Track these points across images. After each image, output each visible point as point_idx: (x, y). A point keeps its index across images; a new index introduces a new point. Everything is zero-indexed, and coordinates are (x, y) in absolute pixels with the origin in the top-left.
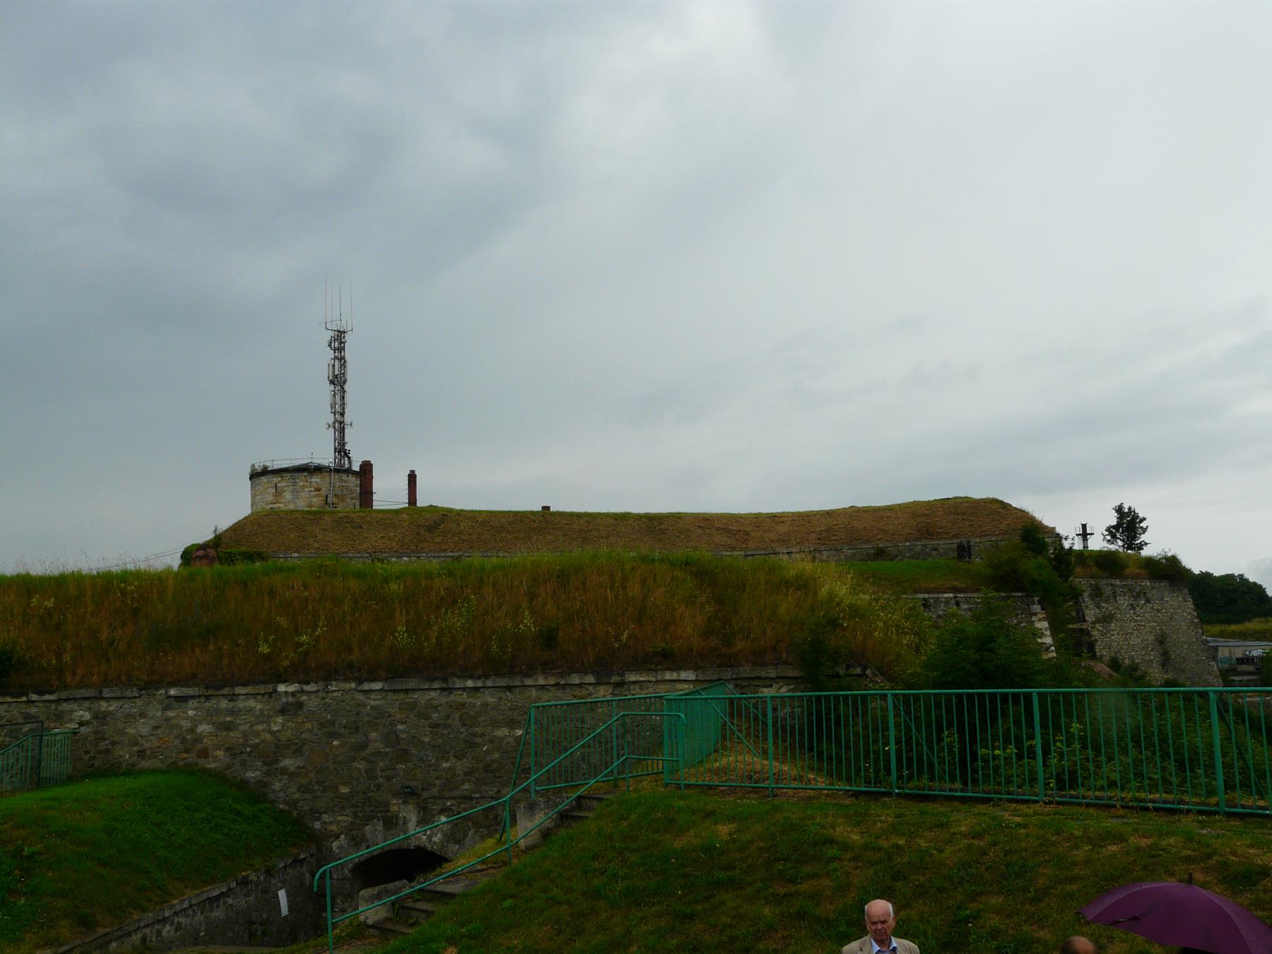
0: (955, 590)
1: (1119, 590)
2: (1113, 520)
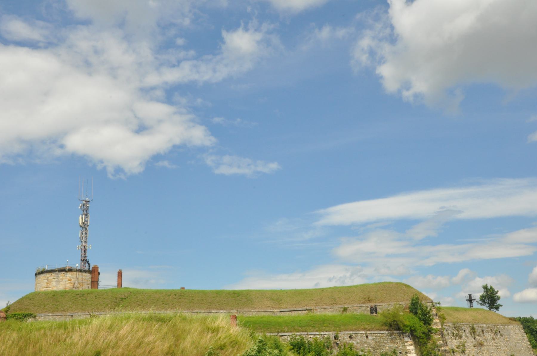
0: (365, 329)
1: (485, 330)
2: (482, 293)
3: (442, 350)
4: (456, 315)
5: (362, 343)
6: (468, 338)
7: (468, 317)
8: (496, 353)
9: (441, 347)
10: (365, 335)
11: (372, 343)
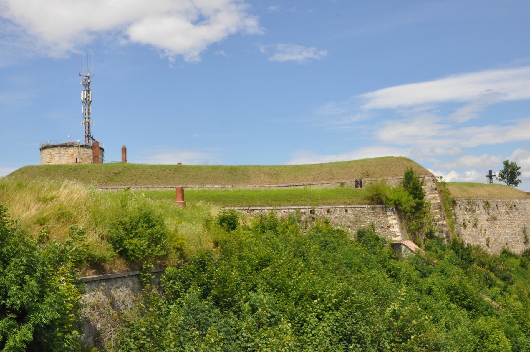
0: (345, 203)
2: (502, 168)
3: (439, 224)
4: (472, 190)
5: (341, 218)
6: (481, 213)
7: (483, 192)
8: (509, 226)
9: (438, 221)
10: (344, 210)
11: (352, 217)
